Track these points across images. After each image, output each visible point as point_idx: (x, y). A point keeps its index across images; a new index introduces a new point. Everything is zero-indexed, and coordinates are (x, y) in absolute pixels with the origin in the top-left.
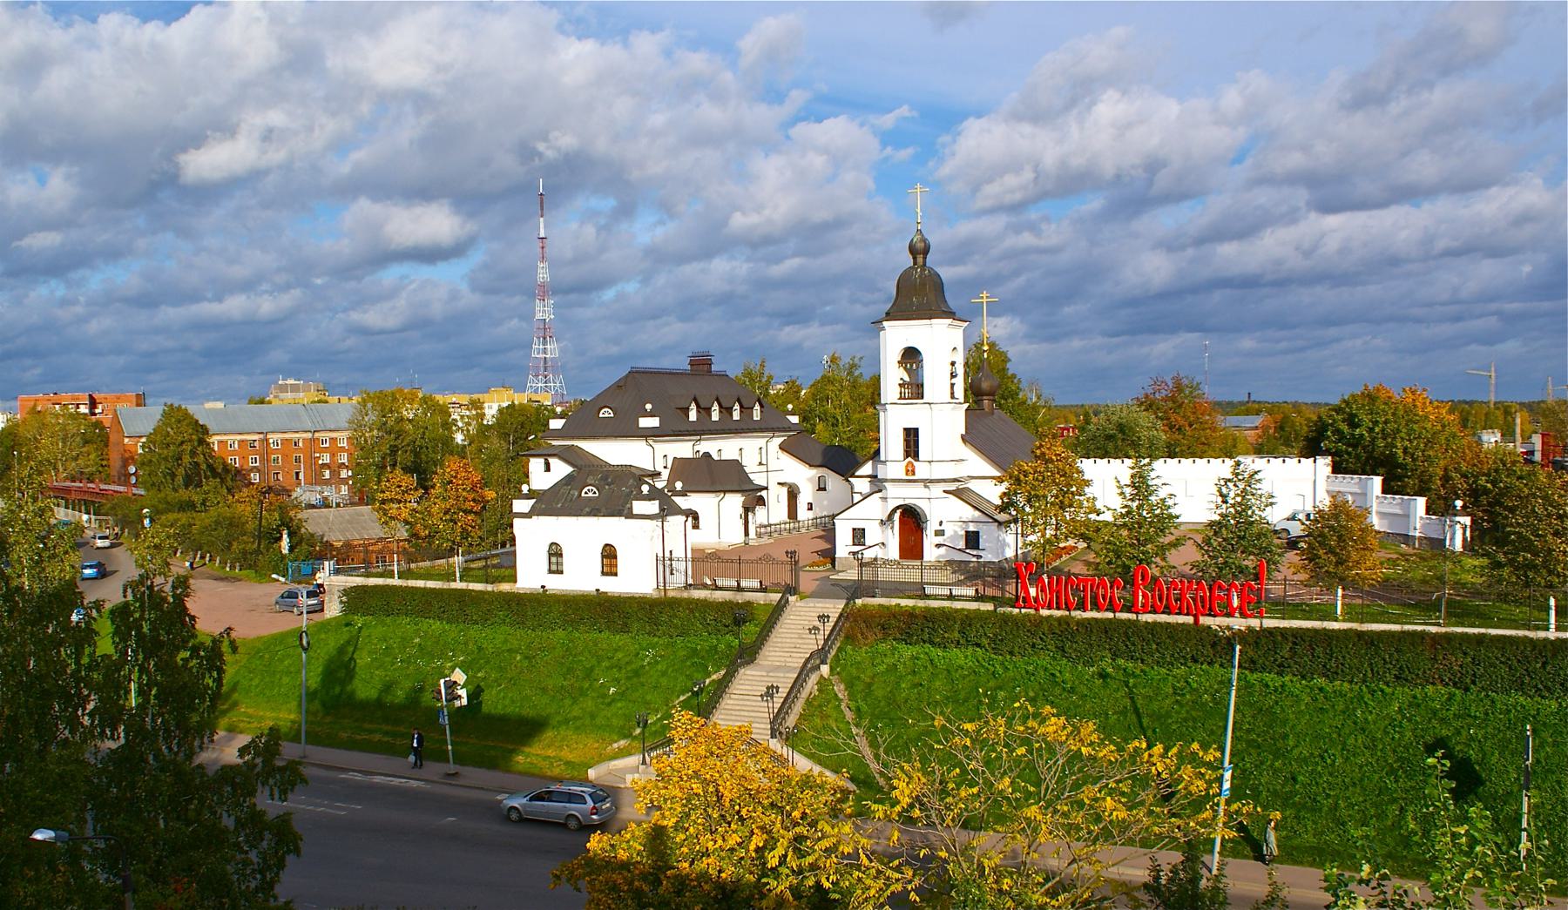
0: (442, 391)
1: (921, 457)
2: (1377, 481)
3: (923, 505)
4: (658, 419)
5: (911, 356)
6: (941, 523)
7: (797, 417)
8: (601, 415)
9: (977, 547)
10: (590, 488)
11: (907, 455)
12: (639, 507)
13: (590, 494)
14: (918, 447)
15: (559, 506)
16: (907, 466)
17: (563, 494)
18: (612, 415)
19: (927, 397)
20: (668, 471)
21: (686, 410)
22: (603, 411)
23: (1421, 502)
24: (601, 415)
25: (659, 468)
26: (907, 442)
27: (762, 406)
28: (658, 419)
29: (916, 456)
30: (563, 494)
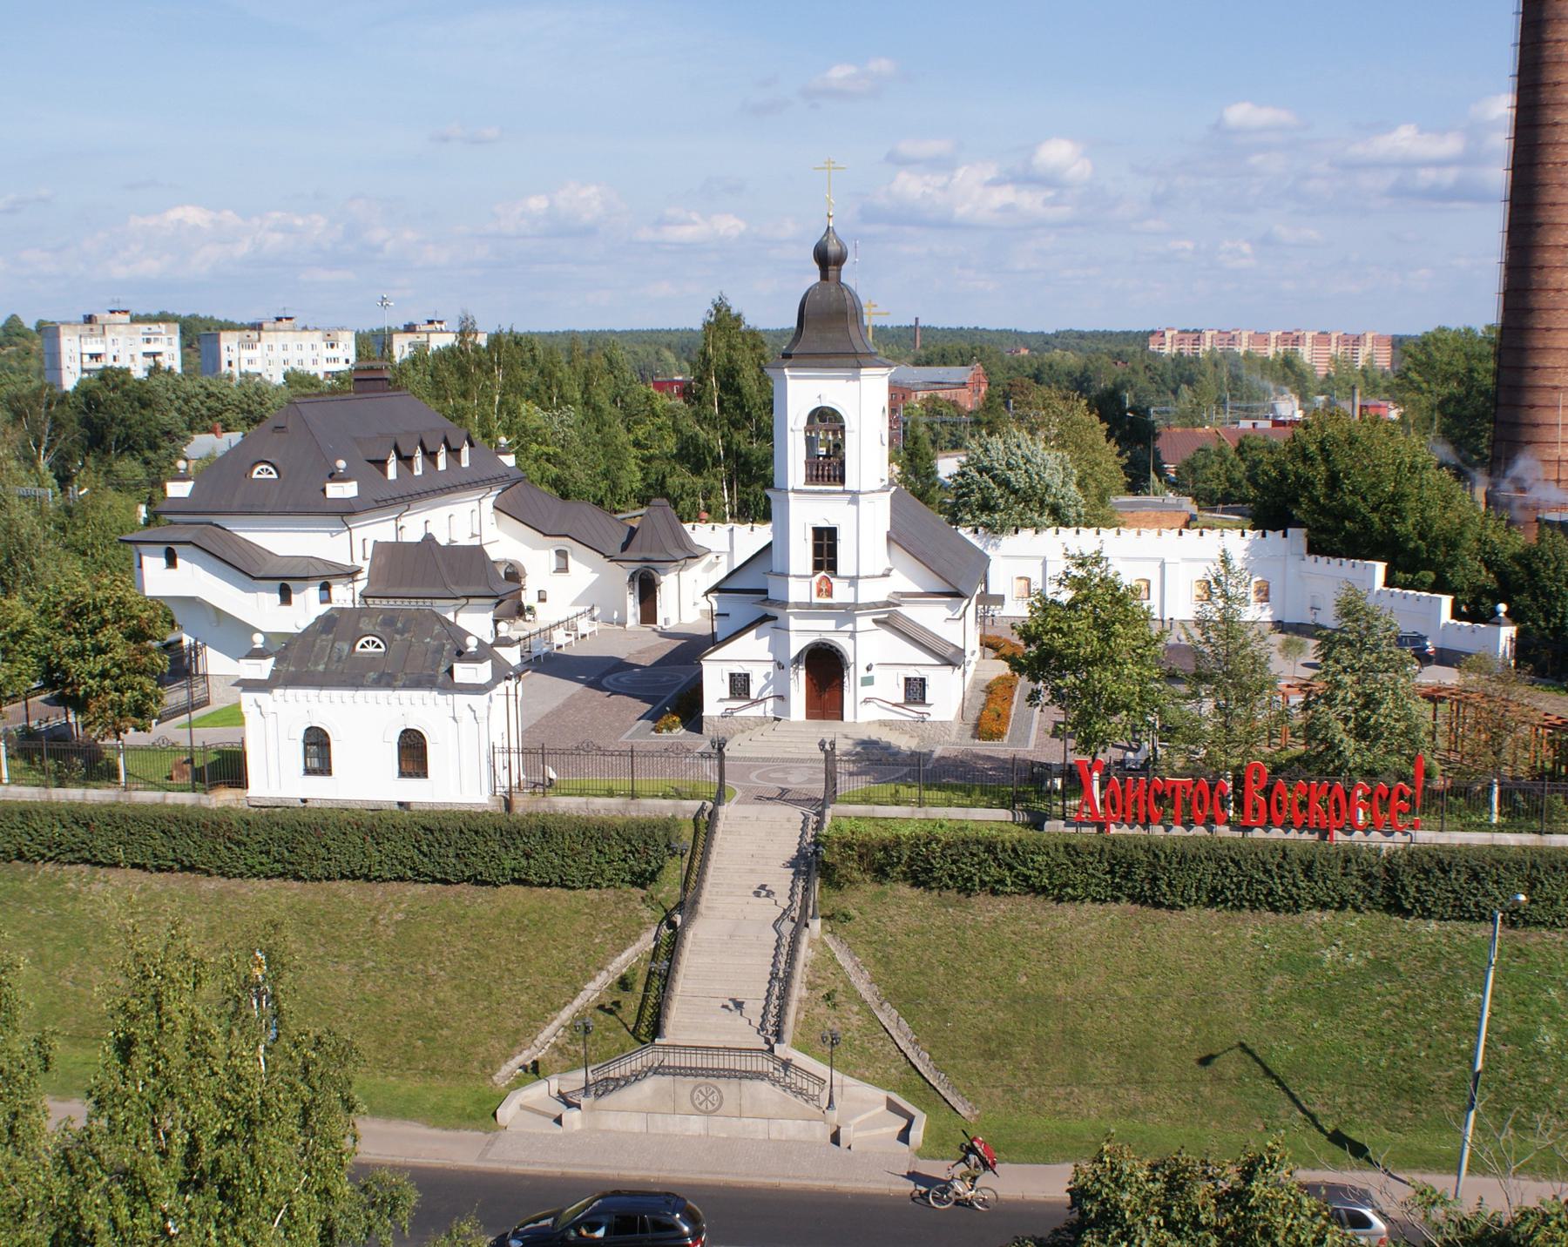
0: (1477, 1114)
1: (841, 570)
2: (1380, 568)
3: (842, 642)
4: (355, 484)
5: (826, 419)
6: (868, 669)
7: (513, 457)
8: (255, 475)
9: (922, 700)
10: (371, 638)
11: (818, 566)
12: (464, 673)
13: (371, 649)
14: (835, 555)
15: (321, 668)
16: (819, 583)
17: (322, 649)
18: (275, 476)
19: (851, 483)
20: (368, 562)
21: (381, 464)
22: (258, 468)
23: (1446, 601)
24: (255, 475)
25: (359, 562)
26: (818, 550)
27: (471, 445)
28: (355, 484)
29: (832, 567)
30: (322, 649)
